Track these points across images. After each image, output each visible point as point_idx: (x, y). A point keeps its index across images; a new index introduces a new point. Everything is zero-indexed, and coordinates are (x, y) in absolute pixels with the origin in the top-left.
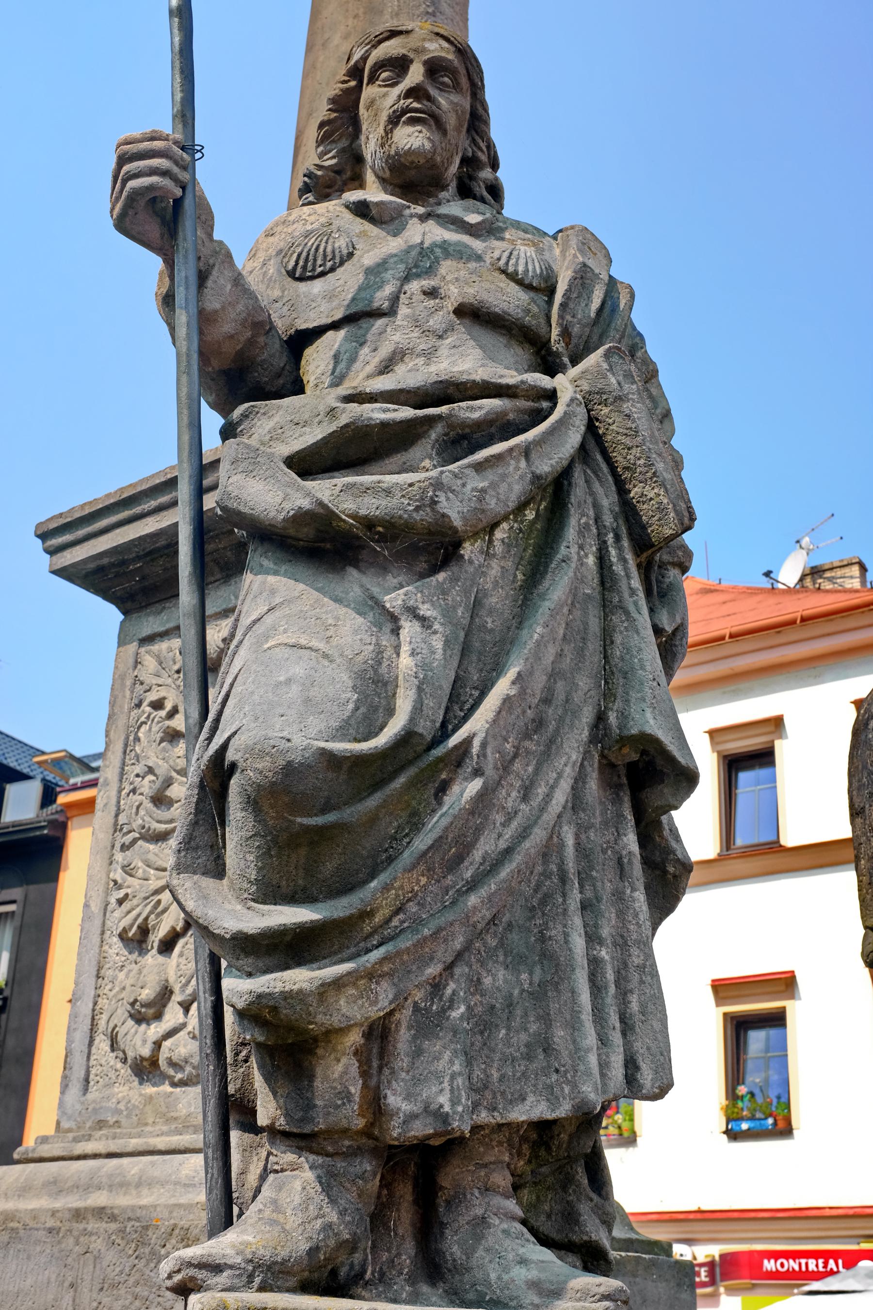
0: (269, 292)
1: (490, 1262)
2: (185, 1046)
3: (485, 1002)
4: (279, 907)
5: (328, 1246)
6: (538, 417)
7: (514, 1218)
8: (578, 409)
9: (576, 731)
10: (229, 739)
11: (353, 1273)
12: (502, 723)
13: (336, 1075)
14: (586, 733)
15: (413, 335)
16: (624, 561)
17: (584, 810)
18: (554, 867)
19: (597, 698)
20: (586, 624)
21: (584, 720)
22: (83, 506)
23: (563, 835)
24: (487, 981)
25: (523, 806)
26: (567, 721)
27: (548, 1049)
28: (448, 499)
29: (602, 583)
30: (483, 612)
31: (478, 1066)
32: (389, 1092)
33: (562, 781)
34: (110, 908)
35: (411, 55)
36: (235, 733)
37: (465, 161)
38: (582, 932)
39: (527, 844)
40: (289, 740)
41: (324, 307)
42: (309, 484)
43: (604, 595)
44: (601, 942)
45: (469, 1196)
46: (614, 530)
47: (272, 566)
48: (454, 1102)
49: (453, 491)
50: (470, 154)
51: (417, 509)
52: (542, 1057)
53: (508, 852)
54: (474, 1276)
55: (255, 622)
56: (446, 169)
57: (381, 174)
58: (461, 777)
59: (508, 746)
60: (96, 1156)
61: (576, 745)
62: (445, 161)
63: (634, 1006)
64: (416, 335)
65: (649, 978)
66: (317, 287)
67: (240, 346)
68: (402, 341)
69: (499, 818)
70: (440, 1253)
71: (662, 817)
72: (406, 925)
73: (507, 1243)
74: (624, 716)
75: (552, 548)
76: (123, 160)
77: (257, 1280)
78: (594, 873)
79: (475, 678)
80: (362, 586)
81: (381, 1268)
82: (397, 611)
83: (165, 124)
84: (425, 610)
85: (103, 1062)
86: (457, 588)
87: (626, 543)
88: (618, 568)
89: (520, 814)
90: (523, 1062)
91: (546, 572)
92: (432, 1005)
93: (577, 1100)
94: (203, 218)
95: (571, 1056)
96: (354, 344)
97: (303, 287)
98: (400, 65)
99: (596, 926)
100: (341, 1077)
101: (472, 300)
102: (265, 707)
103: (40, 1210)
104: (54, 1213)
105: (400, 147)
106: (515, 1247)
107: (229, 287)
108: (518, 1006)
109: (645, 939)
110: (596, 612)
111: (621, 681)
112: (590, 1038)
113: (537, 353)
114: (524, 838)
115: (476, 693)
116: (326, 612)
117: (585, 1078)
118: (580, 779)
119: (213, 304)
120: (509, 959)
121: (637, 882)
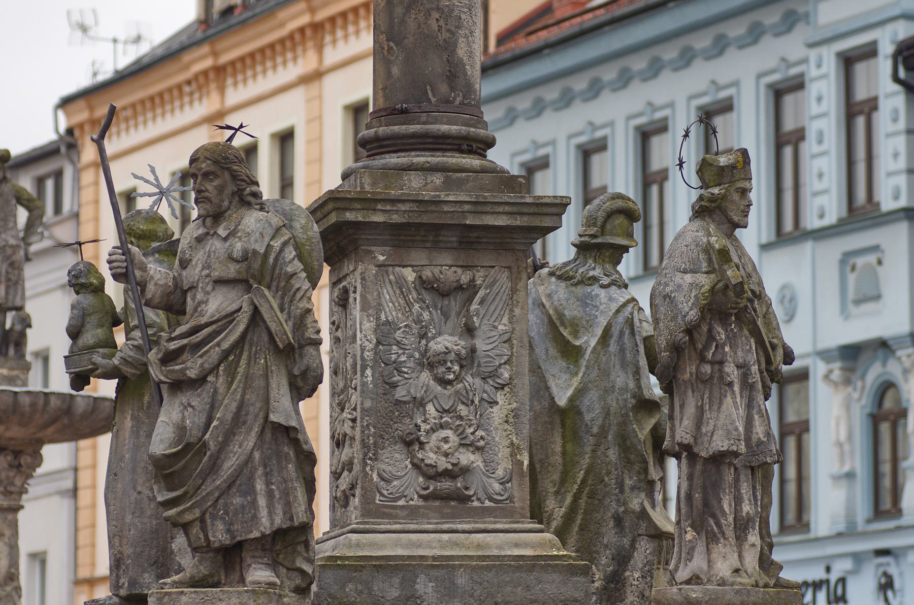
6: (231, 322)
84: (193, 404)
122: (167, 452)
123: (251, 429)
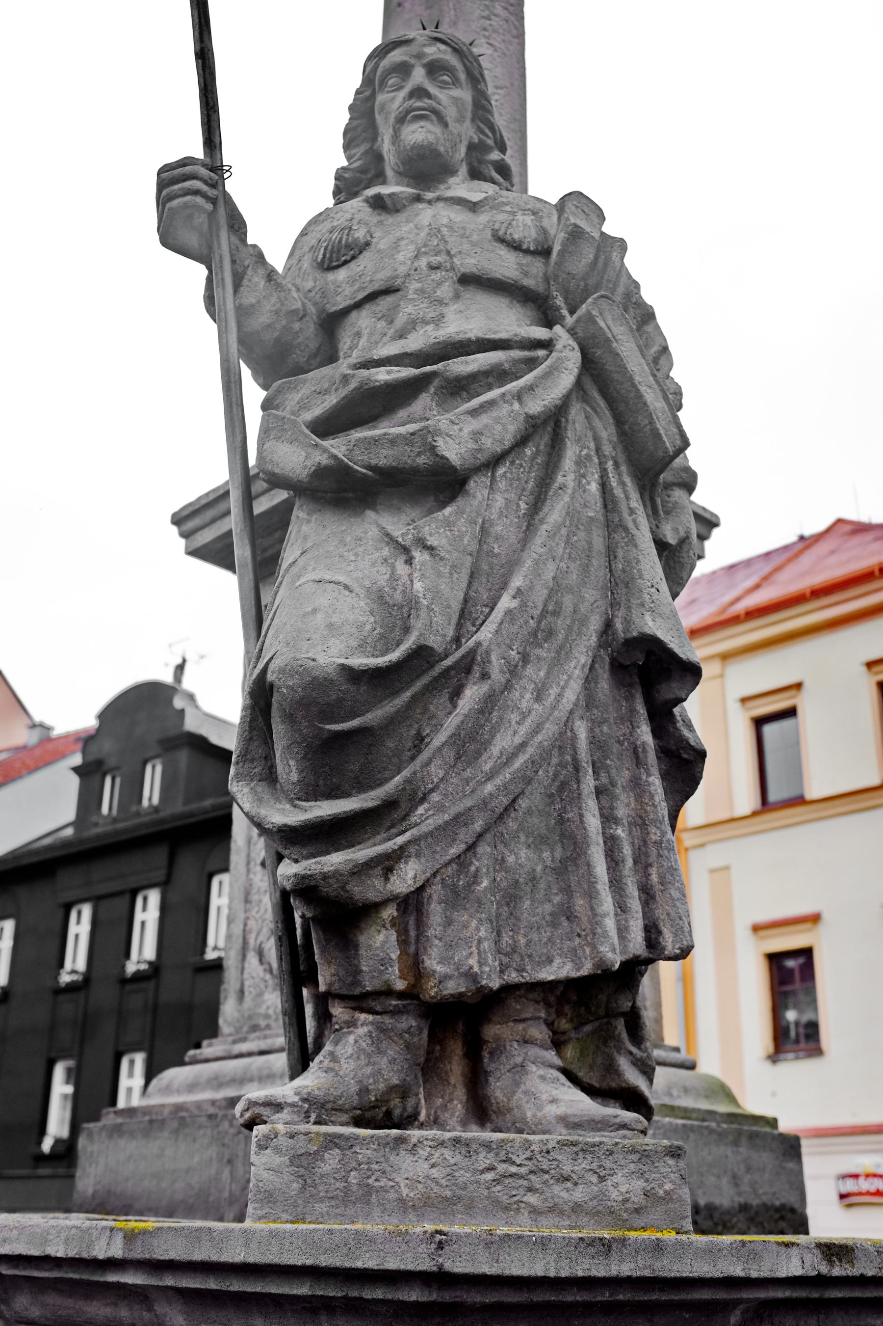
0: (304, 284)
1: (527, 1102)
3: (509, 877)
4: (318, 803)
5: (378, 1090)
6: (532, 364)
7: (552, 1066)
8: (571, 353)
9: (584, 638)
10: (268, 663)
11: (406, 1114)
12: (504, 633)
13: (378, 945)
14: (594, 639)
15: (422, 306)
16: (622, 484)
17: (597, 707)
18: (568, 758)
19: (603, 608)
20: (590, 543)
21: (592, 628)
22: (207, 494)
23: (575, 729)
24: (511, 859)
25: (536, 706)
26: (575, 628)
27: (571, 917)
28: (446, 443)
29: (605, 506)
30: (490, 540)
31: (506, 933)
32: (425, 958)
33: (572, 682)
34: (253, 841)
35: (413, 61)
36: (272, 658)
37: (471, 147)
38: (597, 812)
39: (540, 737)
40: (314, 660)
41: (348, 291)
42: (326, 443)
43: (607, 516)
44: (617, 821)
45: (508, 1048)
46: (613, 458)
47: (305, 517)
48: (481, 965)
49: (450, 436)
50: (476, 140)
52: (566, 924)
53: (523, 745)
54: (514, 1116)
55: (291, 565)
56: (452, 157)
57: (396, 168)
58: (471, 682)
59: (513, 653)
60: (250, 1054)
61: (585, 650)
62: (450, 150)
63: (654, 878)
64: (425, 305)
65: (666, 852)
66: (342, 274)
67: (278, 333)
68: (413, 312)
69: (514, 717)
70: (486, 1098)
71: (674, 710)
72: (430, 813)
73: (542, 1086)
74: (627, 621)
75: (551, 478)
76: (162, 185)
77: (313, 1117)
78: (608, 762)
79: (485, 597)
80: (378, 526)
81: (436, 1112)
82: (407, 543)
83: (198, 152)
84: (432, 541)
85: (254, 975)
86: (463, 520)
87: (624, 468)
88: (618, 492)
89: (534, 712)
90: (549, 929)
91: (545, 499)
92: (458, 881)
93: (597, 959)
94: (236, 227)
95: (590, 922)
96: (374, 319)
97: (331, 276)
98: (404, 70)
99: (612, 808)
100: (382, 946)
101: (474, 270)
102: (294, 634)
103: (203, 1101)
104: (213, 1102)
105: (407, 143)
106: (549, 1089)
107: (263, 283)
108: (542, 881)
109: (661, 818)
110: (600, 532)
111: (624, 590)
112: (607, 903)
113: (539, 308)
114: (537, 733)
115: (487, 610)
116: (349, 551)
117: (602, 940)
118: (589, 681)
119: (248, 298)
120: (531, 840)
121: (651, 768)
122: (358, 661)
123: (562, 654)
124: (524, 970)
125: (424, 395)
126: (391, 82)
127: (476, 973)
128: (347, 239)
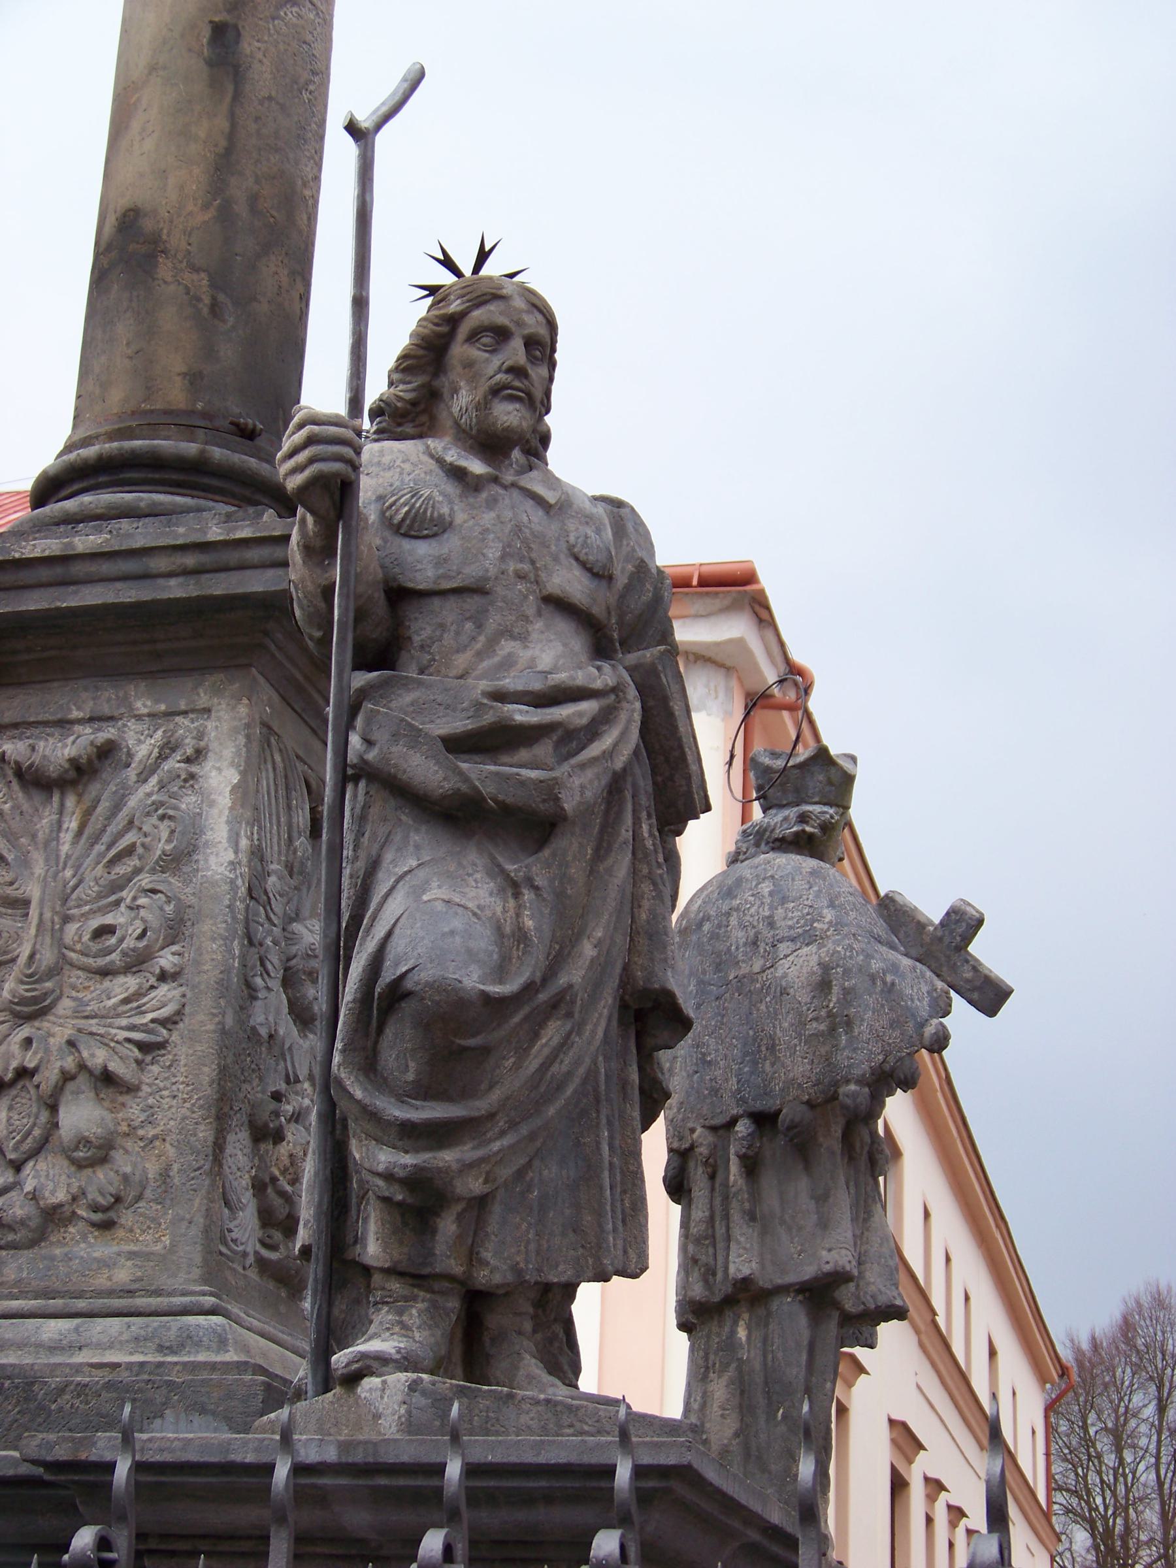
2: (21, 1207)
48: (527, 1262)
51: (544, 801)
84: (539, 882)
124: (542, 1271)
125: (547, 741)
126: (484, 340)
127: (522, 1270)
128: (432, 513)
